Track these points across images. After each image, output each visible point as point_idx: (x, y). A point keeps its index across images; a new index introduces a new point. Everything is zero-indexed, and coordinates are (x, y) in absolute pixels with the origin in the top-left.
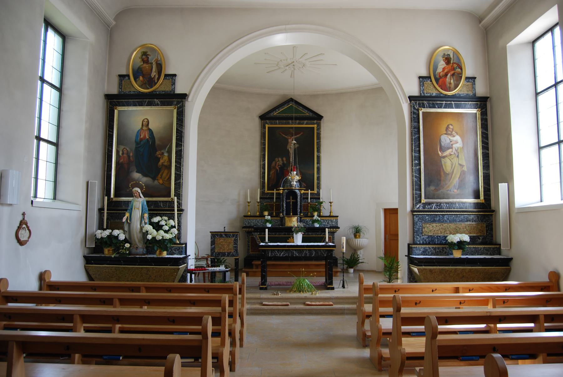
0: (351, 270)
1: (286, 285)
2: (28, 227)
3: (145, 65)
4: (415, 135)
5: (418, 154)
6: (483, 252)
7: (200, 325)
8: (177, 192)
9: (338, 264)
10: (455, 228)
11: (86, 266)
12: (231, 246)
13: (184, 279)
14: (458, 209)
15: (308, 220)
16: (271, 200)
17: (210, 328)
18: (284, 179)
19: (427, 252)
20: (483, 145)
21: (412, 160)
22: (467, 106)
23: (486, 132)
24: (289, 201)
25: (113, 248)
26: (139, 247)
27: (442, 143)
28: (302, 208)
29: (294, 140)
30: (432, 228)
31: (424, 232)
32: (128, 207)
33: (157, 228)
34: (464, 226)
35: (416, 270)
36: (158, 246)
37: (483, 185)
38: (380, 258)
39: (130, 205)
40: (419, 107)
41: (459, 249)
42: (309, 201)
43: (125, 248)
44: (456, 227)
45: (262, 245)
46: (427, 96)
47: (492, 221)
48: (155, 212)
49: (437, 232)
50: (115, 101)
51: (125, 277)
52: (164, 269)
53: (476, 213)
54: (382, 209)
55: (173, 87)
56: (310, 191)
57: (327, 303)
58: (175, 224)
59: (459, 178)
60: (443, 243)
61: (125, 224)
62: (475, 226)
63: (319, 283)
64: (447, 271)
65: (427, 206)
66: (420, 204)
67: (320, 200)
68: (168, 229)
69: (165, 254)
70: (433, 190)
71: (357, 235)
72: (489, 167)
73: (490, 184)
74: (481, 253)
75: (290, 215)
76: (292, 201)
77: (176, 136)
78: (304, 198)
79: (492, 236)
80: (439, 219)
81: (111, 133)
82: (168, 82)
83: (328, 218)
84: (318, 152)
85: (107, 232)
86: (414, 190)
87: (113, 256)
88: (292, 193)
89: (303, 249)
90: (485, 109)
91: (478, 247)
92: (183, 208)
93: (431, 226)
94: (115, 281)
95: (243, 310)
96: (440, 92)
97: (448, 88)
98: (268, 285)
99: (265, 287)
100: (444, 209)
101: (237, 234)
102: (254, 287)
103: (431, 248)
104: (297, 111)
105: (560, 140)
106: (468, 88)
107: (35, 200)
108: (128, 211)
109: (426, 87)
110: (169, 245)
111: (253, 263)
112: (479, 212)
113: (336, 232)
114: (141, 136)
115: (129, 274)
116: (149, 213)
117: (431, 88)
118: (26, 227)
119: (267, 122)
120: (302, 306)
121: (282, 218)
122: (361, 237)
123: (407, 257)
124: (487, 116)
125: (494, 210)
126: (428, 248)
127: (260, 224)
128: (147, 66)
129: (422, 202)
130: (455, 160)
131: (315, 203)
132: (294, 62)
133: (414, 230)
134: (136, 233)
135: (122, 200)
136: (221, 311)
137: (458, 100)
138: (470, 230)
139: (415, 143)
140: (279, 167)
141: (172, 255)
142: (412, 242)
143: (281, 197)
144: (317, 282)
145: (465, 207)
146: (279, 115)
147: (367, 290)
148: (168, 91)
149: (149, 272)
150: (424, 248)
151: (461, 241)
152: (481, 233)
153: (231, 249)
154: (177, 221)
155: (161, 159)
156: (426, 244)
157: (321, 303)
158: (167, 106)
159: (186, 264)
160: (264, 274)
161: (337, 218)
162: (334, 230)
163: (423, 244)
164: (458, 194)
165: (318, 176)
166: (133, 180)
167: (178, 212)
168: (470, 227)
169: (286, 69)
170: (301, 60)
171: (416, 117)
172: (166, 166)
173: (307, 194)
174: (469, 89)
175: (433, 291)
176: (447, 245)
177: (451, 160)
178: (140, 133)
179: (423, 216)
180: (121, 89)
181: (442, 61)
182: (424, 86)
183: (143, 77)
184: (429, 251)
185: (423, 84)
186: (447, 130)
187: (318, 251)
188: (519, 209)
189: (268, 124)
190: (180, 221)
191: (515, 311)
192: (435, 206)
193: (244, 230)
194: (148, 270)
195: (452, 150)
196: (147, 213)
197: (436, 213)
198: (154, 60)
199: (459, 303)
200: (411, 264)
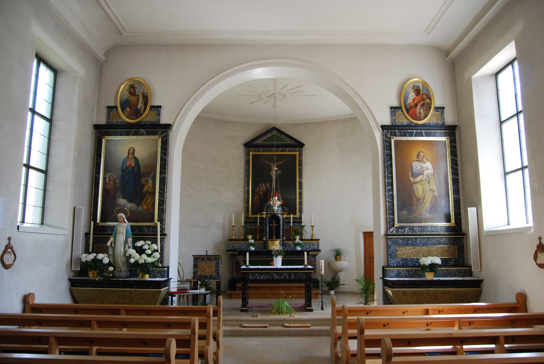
0: (332, 292)
1: (267, 307)
2: (13, 251)
3: (132, 97)
5: (391, 180)
6: (455, 274)
7: (164, 347)
8: (160, 217)
10: (427, 251)
12: (213, 269)
13: (165, 301)
14: (430, 232)
15: (290, 243)
16: (255, 224)
17: (174, 350)
18: (267, 204)
19: (401, 275)
20: (453, 171)
22: (437, 134)
23: (456, 159)
24: (272, 225)
25: (98, 271)
27: (413, 170)
28: (285, 231)
29: (275, 167)
31: (397, 255)
32: (113, 231)
33: (140, 252)
34: (436, 249)
35: (390, 292)
36: (140, 270)
37: (454, 209)
38: (356, 280)
40: (392, 135)
41: (431, 271)
42: (292, 225)
43: (108, 271)
44: (429, 250)
46: (398, 125)
47: (463, 244)
49: (410, 255)
51: (109, 299)
52: (146, 291)
53: (447, 237)
54: (362, 232)
55: (158, 118)
56: (293, 215)
57: (305, 325)
58: (158, 248)
59: (430, 203)
61: (110, 248)
63: (299, 305)
64: (420, 293)
65: (400, 230)
66: (393, 228)
67: (302, 224)
68: (151, 253)
69: (147, 278)
71: (337, 258)
73: (460, 208)
74: (453, 274)
75: (273, 238)
76: (275, 225)
77: (160, 164)
78: (286, 222)
79: (464, 259)
80: (412, 242)
81: (99, 161)
82: (154, 113)
83: (309, 241)
84: (300, 178)
85: (92, 256)
88: (275, 218)
89: (283, 272)
90: (454, 136)
91: (450, 269)
92: (166, 232)
93: (404, 249)
94: (98, 304)
95: (219, 332)
96: (410, 121)
97: (418, 118)
99: (246, 309)
100: (416, 232)
101: (219, 258)
103: (405, 271)
104: (279, 139)
105: (523, 166)
107: (23, 225)
108: (113, 235)
110: (151, 269)
111: (236, 285)
113: (317, 255)
114: (127, 164)
115: (113, 297)
116: (133, 238)
117: (402, 118)
118: (11, 251)
120: (280, 328)
121: (265, 241)
122: (341, 260)
123: (381, 280)
124: (456, 143)
125: (465, 233)
126: (401, 271)
127: (244, 248)
128: (134, 98)
129: (395, 226)
130: (426, 186)
131: (297, 226)
132: (275, 93)
133: (388, 253)
134: (120, 256)
135: (108, 225)
136: (191, 334)
137: (428, 129)
138: (442, 253)
139: (388, 170)
140: (263, 192)
141: (154, 278)
142: (386, 265)
143: (264, 221)
144: (297, 304)
145: (437, 230)
146: (262, 143)
147: (339, 312)
148: (153, 122)
149: (131, 294)
150: (398, 271)
151: (433, 263)
152: (452, 255)
153: (212, 272)
154: (160, 245)
155: (146, 186)
156: (400, 267)
157: (299, 325)
158: (152, 135)
159: (168, 287)
160: (245, 296)
161: (318, 241)
162: (316, 253)
163: (397, 267)
164: (430, 218)
166: (119, 205)
167: (161, 237)
168: (442, 250)
170: (281, 91)
171: (388, 145)
173: (289, 219)
175: (403, 313)
176: (420, 267)
177: (423, 186)
178: (126, 161)
179: (397, 239)
180: (109, 119)
181: (412, 92)
183: (130, 108)
184: (403, 273)
185: (395, 114)
187: (297, 274)
188: (488, 232)
189: (252, 152)
190: (163, 245)
191: (476, 333)
192: (408, 230)
193: (229, 253)
194: (131, 292)
196: (130, 238)
197: (409, 237)
198: (141, 92)
199: (426, 325)
200: (386, 286)
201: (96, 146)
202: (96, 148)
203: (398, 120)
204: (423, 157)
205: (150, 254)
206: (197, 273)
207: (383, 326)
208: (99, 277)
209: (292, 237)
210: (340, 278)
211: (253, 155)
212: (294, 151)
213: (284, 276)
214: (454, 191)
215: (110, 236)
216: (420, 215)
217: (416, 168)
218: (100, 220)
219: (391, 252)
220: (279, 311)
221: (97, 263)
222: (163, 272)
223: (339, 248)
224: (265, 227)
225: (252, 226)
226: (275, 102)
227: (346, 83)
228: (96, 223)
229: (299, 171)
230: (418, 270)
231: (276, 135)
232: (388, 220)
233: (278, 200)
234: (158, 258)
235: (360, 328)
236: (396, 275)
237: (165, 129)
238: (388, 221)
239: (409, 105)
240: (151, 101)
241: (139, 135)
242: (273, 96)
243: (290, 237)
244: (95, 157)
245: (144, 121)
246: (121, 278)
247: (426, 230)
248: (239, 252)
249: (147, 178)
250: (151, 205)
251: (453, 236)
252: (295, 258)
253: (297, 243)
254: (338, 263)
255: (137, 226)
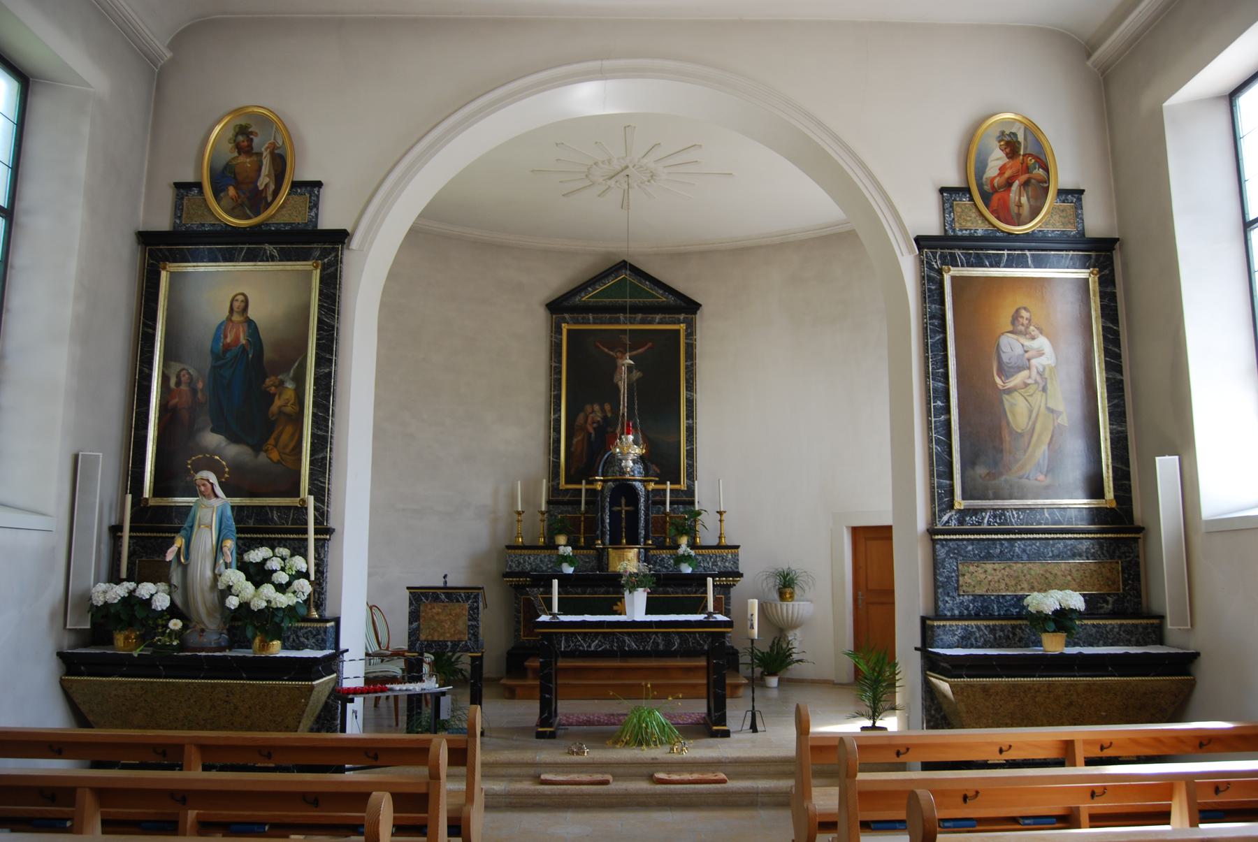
0: (773, 681)
1: (607, 724)
3: (242, 159)
4: (933, 335)
6: (1118, 636)
8: (316, 482)
9: (741, 666)
10: (1042, 575)
11: (65, 680)
12: (462, 624)
15: (664, 556)
16: (575, 506)
18: (606, 456)
19: (973, 640)
20: (1107, 359)
21: (927, 400)
23: (1115, 328)
24: (619, 508)
25: (139, 630)
26: (207, 627)
29: (628, 358)
30: (983, 576)
31: (962, 586)
33: (258, 579)
34: (1066, 570)
35: (944, 686)
36: (257, 628)
37: (1113, 463)
39: (192, 513)
41: (1059, 632)
42: (668, 510)
43: (168, 631)
44: (1046, 571)
45: (544, 622)
46: (962, 236)
47: (1138, 556)
48: (259, 536)
49: (996, 585)
50: (161, 249)
51: (169, 708)
52: (273, 687)
53: (1096, 536)
54: (847, 527)
55: (313, 214)
56: (671, 484)
57: (710, 776)
58: (308, 569)
60: (1013, 615)
61: (174, 566)
62: (1094, 568)
64: (1027, 689)
65: (968, 519)
67: (694, 507)
68: (288, 580)
69: (276, 649)
70: (983, 476)
71: (785, 594)
72: (1125, 417)
73: (1128, 459)
75: (620, 543)
76: (624, 508)
77: (317, 339)
78: (654, 503)
79: (1139, 596)
80: (1001, 552)
81: (150, 331)
82: (301, 201)
83: (713, 551)
84: (689, 391)
85: (121, 590)
86: (934, 477)
87: (135, 654)
88: (625, 490)
90: (1110, 268)
96: (994, 226)
97: (1015, 216)
98: (560, 724)
99: (550, 732)
102: (521, 731)
103: (983, 628)
104: (636, 291)
106: (1065, 218)
108: (183, 532)
109: (959, 214)
110: (286, 624)
111: (527, 664)
112: (1103, 533)
113: (734, 585)
114: (226, 337)
116: (239, 539)
119: (564, 318)
120: (643, 786)
121: (600, 551)
122: (795, 597)
123: (919, 653)
124: (1115, 286)
126: (975, 629)
127: (546, 567)
128: (248, 160)
129: (957, 506)
130: (1038, 400)
132: (627, 167)
133: (935, 580)
134: (202, 590)
135: (173, 504)
136: (428, 780)
138: (1082, 580)
139: (934, 356)
140: (595, 425)
141: (298, 649)
142: (931, 613)
143: (599, 498)
144: (685, 714)
146: (594, 302)
148: (298, 223)
150: (965, 628)
151: (1065, 609)
152: (1109, 585)
153: (460, 632)
154: (315, 558)
155: (277, 397)
156: (969, 618)
157: (695, 776)
158: (295, 261)
159: (335, 675)
161: (736, 550)
162: (730, 581)
164: (1047, 487)
165: (688, 448)
166: (204, 450)
167: (319, 536)
169: (609, 187)
170: (645, 161)
171: (936, 289)
172: (288, 416)
173: (662, 493)
174: (1067, 219)
176: (1026, 619)
177: (1029, 398)
178: (225, 330)
179: (960, 543)
180: (180, 218)
182: (953, 211)
183: (236, 188)
184: (978, 635)
185: (952, 206)
186: (1016, 322)
189: (568, 323)
190: (322, 560)
192: (990, 517)
193: (507, 581)
195: (1030, 372)
197: (993, 536)
198: (266, 145)
199: (1089, 795)
200: (930, 671)
201: (143, 290)
202: (142, 295)
203: (961, 224)
204: (1027, 322)
205: (284, 582)
206: (419, 634)
207: (960, 800)
208: (142, 647)
209: (668, 540)
210: (792, 644)
211: (569, 331)
212: (674, 323)
213: (653, 642)
214: (1110, 414)
215: (175, 535)
216: (1021, 478)
217: (1009, 350)
218: (152, 491)
219: (946, 578)
220: (640, 737)
221: (135, 608)
222: (323, 634)
223: (789, 568)
224: (600, 514)
225: (567, 512)
226: (626, 191)
227: (820, 124)
228: (140, 500)
229: (686, 373)
230: (1020, 627)
231: (631, 282)
232: (936, 490)
233: (635, 442)
234: (309, 595)
235: (924, 826)
236: (961, 641)
237: (331, 243)
238: (936, 494)
239: (989, 182)
240: (293, 169)
241: (260, 261)
242: (622, 173)
243: (665, 541)
244: (140, 319)
245: (274, 221)
246: (202, 650)
247: (1038, 517)
248: (532, 577)
249: (280, 377)
250: (293, 449)
251: (1110, 535)
252: (677, 593)
253: (683, 555)
254: (787, 605)
255: (253, 507)
